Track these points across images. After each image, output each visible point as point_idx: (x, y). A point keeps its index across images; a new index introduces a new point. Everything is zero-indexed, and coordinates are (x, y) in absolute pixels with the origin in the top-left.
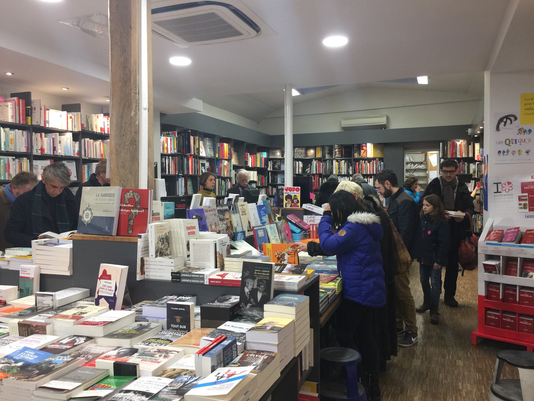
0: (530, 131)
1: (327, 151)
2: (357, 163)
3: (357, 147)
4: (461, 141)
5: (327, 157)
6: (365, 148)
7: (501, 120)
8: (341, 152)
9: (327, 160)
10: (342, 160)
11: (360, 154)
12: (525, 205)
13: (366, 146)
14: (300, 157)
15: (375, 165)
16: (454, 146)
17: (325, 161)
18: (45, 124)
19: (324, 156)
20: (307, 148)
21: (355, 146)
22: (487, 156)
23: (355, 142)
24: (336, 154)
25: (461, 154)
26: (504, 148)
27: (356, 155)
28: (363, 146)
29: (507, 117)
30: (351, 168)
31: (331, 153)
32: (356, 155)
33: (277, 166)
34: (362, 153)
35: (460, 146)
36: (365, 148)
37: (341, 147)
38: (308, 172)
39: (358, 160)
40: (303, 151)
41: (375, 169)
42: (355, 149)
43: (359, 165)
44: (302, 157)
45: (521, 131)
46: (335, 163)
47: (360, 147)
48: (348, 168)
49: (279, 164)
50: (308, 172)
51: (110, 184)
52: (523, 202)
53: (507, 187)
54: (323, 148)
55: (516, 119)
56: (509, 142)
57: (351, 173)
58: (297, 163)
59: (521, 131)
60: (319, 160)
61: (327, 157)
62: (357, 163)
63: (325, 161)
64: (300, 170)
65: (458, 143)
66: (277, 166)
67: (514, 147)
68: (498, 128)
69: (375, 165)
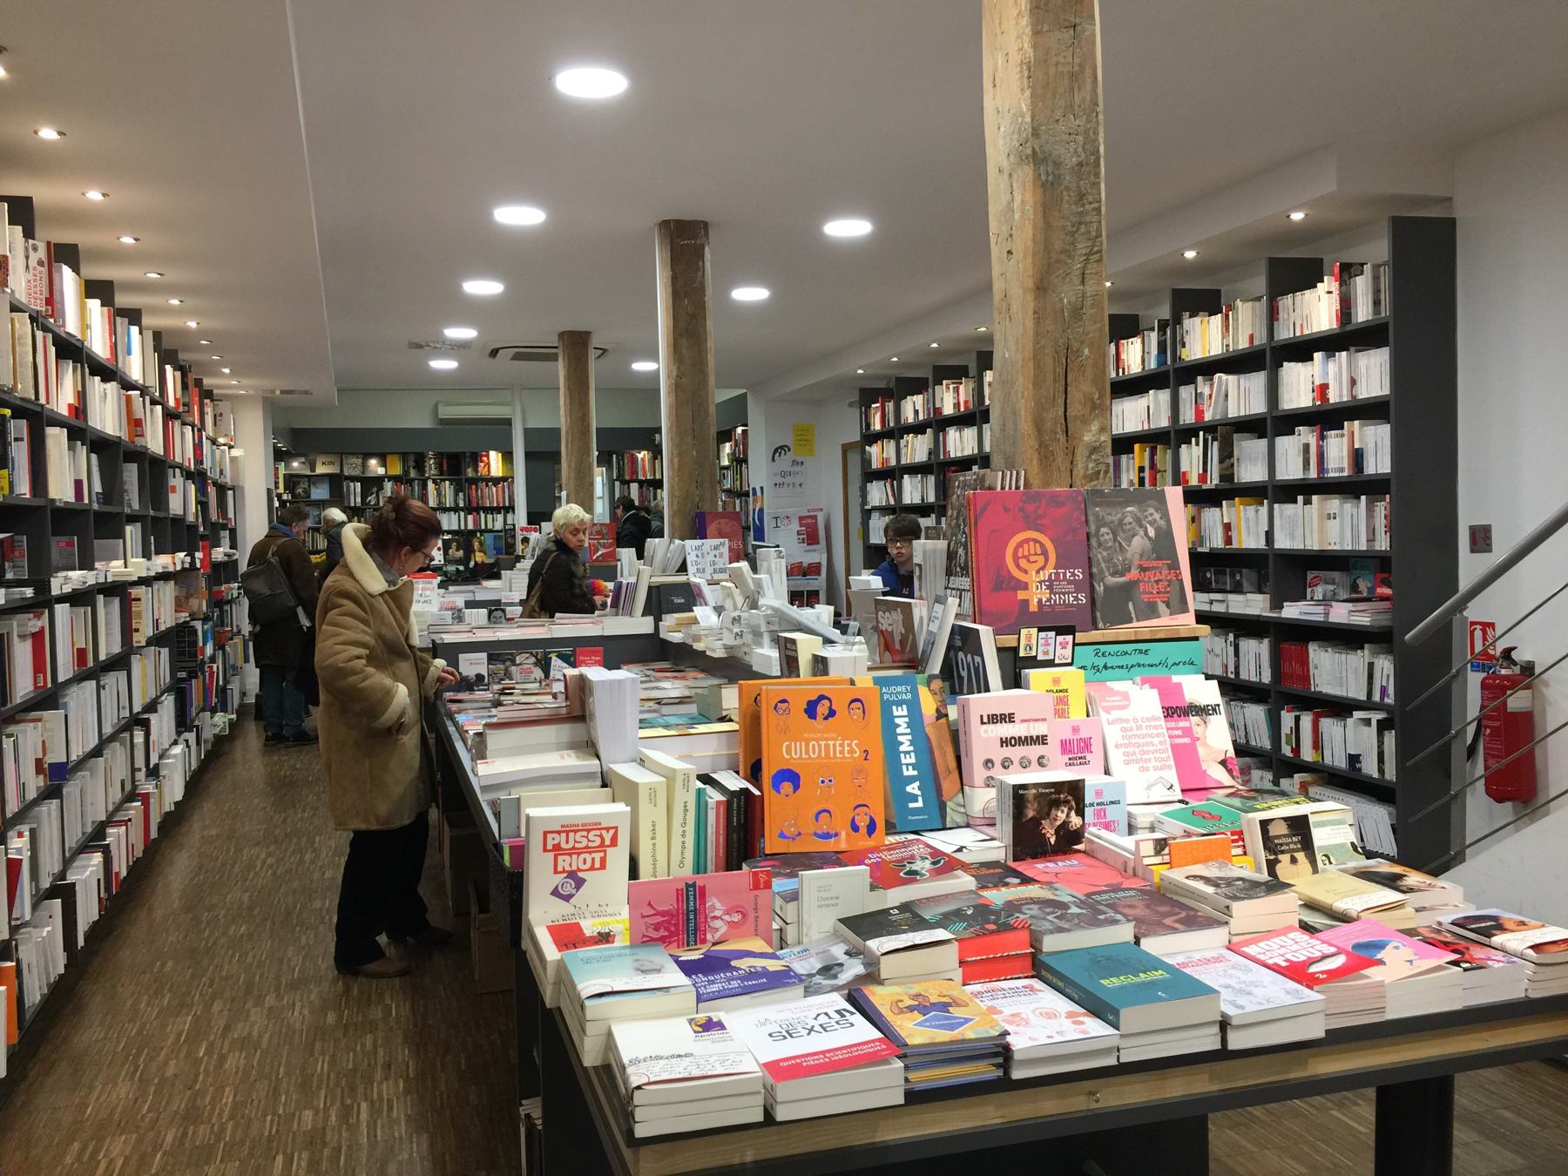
0: (802, 463)
1: (412, 463)
2: (474, 487)
3: (471, 457)
4: (643, 453)
5: (413, 474)
6: (485, 459)
7: (776, 451)
8: (440, 466)
9: (413, 480)
10: (444, 480)
11: (476, 470)
12: (803, 539)
13: (488, 456)
14: (353, 474)
15: (506, 490)
16: (634, 460)
17: (410, 482)
18: (1228, 540)
19: (406, 472)
20: (367, 456)
21: (468, 455)
22: (762, 488)
23: (467, 448)
24: (430, 469)
25: (645, 474)
26: (779, 480)
27: (470, 473)
28: (482, 456)
29: (781, 447)
30: (461, 495)
31: (420, 467)
32: (470, 473)
33: (300, 490)
34: (480, 469)
35: (643, 460)
36: (485, 459)
37: (440, 456)
38: (372, 503)
39: (475, 481)
40: (360, 460)
41: (507, 498)
42: (468, 460)
43: (477, 491)
44: (356, 472)
45: (795, 463)
46: (431, 486)
47: (475, 458)
48: (456, 495)
49: (306, 486)
50: (372, 503)
51: (1186, 502)
52: (801, 537)
53: (786, 521)
54: (404, 456)
55: (789, 450)
56: (783, 474)
57: (462, 504)
58: (352, 484)
59: (795, 463)
60: (396, 479)
61: (413, 474)
62: (474, 487)
63: (410, 482)
64: (359, 500)
65: (640, 456)
66: (300, 490)
67: (789, 480)
68: (773, 460)
69: (506, 490)
